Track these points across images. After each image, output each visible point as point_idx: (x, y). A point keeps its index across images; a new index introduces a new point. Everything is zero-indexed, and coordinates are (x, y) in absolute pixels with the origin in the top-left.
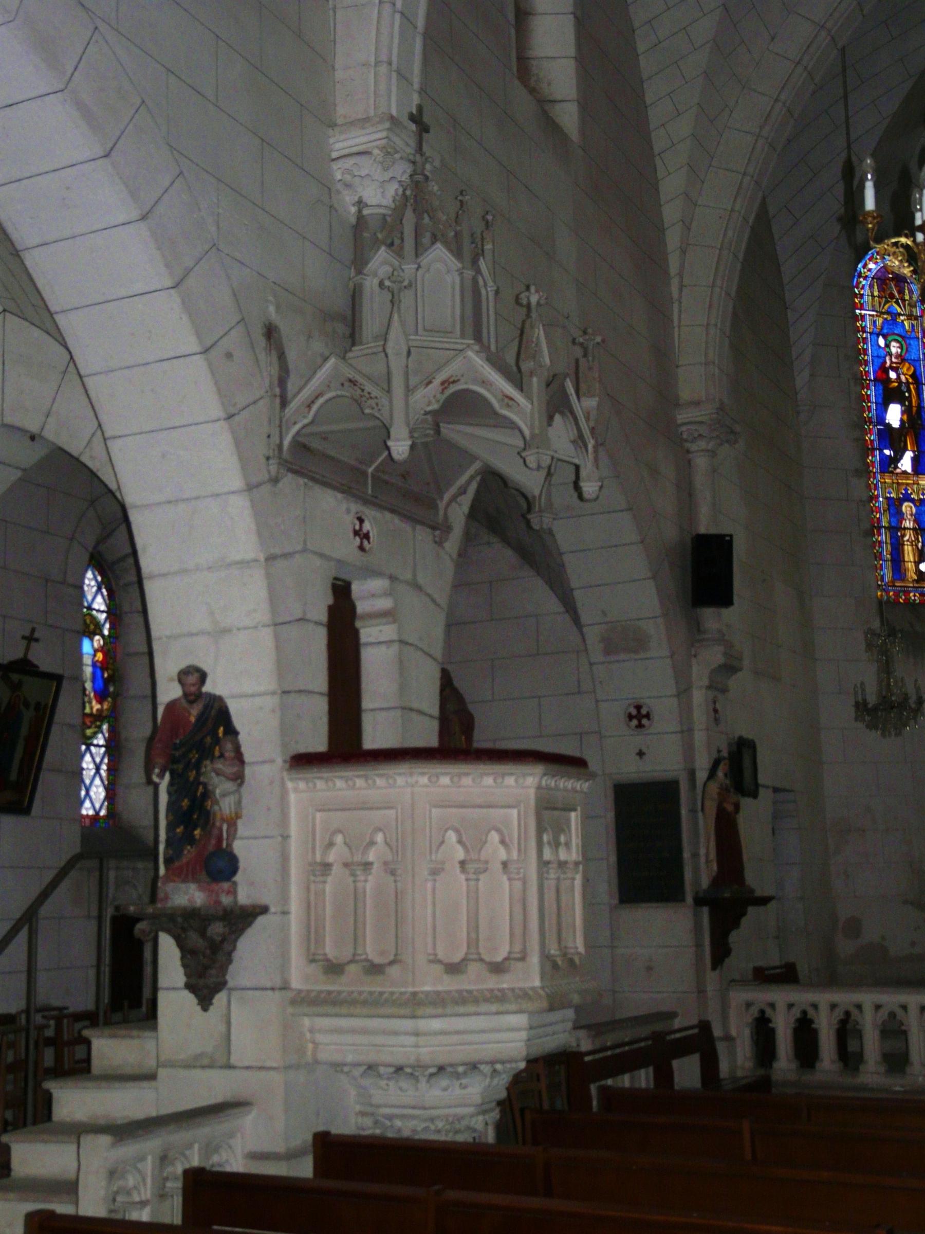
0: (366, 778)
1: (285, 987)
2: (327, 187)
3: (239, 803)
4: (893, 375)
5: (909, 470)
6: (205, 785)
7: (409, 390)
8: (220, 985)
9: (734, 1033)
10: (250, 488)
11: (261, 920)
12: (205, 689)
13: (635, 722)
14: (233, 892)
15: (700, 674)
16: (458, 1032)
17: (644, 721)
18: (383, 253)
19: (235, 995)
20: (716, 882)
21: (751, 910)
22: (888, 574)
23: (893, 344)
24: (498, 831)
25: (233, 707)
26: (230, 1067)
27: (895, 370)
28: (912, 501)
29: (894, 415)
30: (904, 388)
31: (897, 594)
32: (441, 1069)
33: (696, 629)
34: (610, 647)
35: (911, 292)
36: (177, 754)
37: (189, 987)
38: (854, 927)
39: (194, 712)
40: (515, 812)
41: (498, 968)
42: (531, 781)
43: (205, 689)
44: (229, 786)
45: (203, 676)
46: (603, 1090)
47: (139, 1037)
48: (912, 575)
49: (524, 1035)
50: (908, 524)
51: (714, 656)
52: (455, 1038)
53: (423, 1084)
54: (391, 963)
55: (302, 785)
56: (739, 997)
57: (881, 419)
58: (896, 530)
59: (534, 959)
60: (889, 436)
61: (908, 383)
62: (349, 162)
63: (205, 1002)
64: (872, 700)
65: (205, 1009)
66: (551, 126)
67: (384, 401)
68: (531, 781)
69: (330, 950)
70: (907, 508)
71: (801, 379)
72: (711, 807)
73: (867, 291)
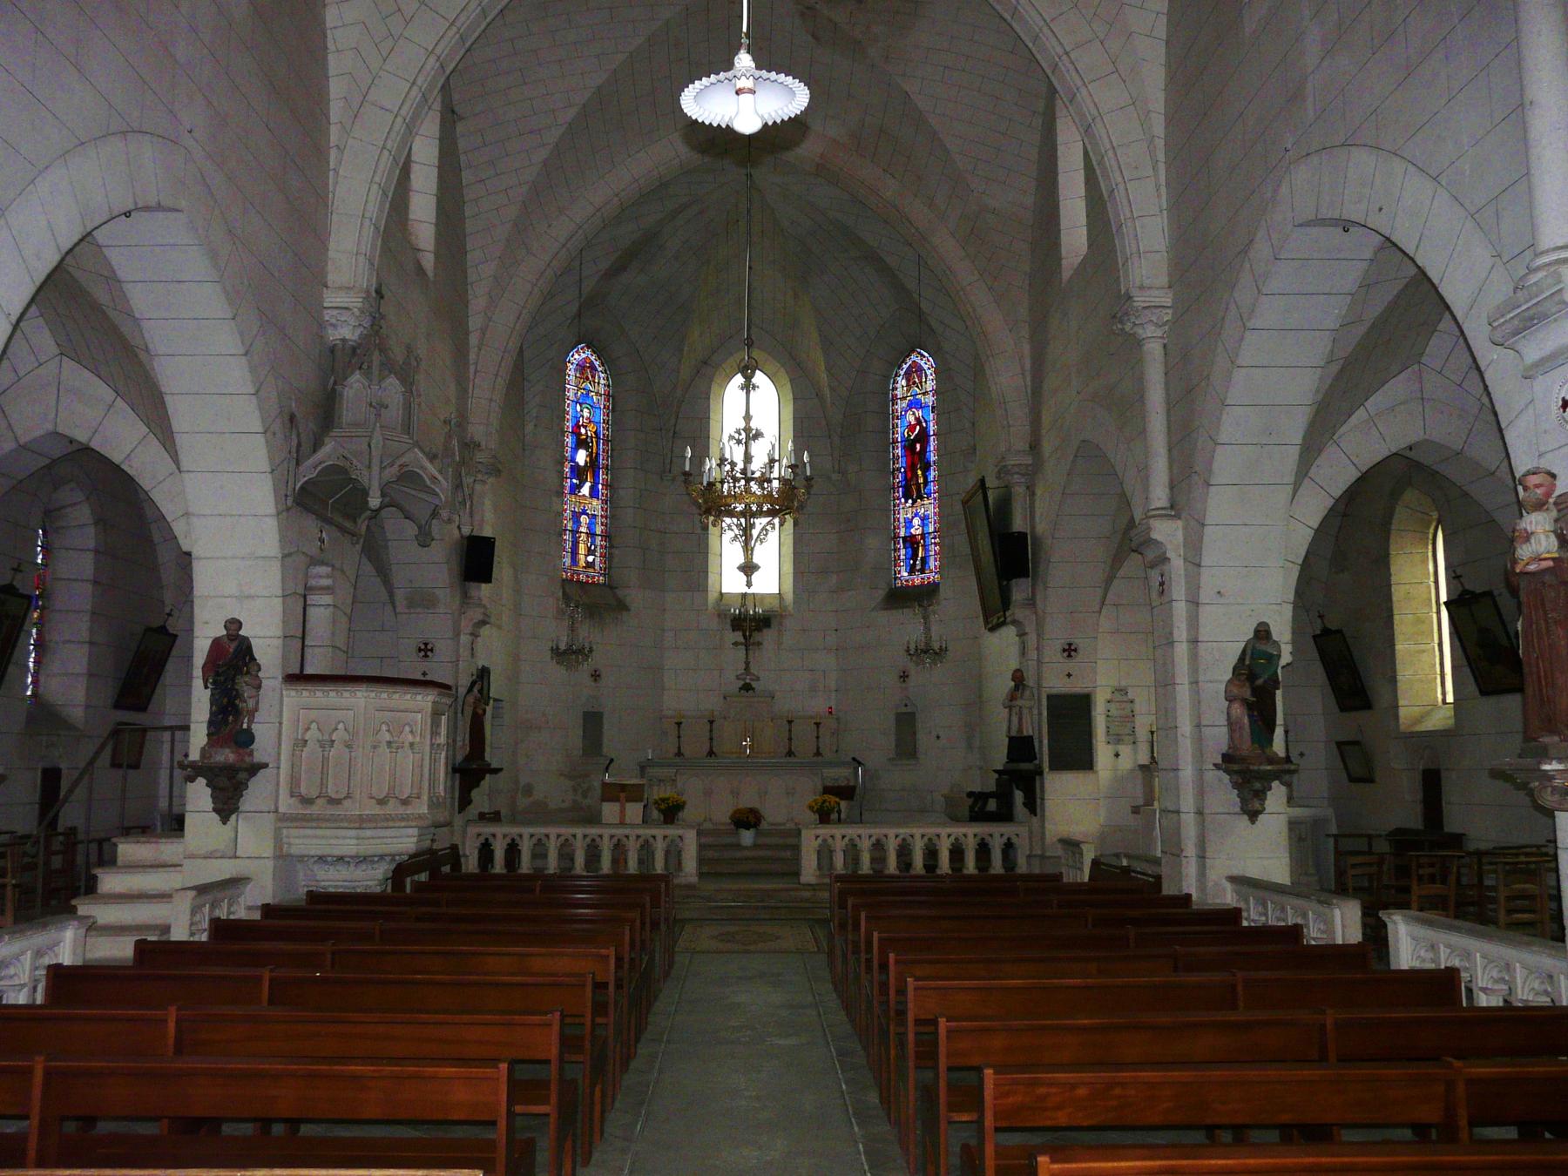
0: (337, 692)
1: (276, 811)
2: (322, 325)
3: (257, 703)
4: (583, 431)
5: (587, 494)
6: (237, 690)
7: (382, 469)
8: (235, 810)
9: (468, 853)
10: (278, 514)
11: (262, 773)
12: (241, 633)
13: (423, 653)
14: (251, 754)
15: (466, 625)
16: (379, 838)
17: (429, 653)
18: (357, 376)
19: (242, 816)
20: (467, 759)
21: (488, 776)
22: (568, 561)
23: (585, 410)
24: (410, 726)
25: (253, 642)
26: (236, 857)
27: (585, 427)
28: (587, 514)
29: (581, 457)
30: (589, 440)
31: (572, 575)
32: (365, 858)
33: (465, 595)
34: (411, 603)
35: (599, 377)
36: (220, 671)
37: (215, 810)
38: (528, 790)
39: (232, 647)
40: (420, 715)
41: (405, 802)
42: (430, 698)
43: (241, 633)
44: (253, 692)
45: (239, 624)
46: (412, 881)
47: (156, 842)
48: (582, 563)
49: (415, 840)
50: (583, 529)
51: (476, 614)
52: (379, 841)
53: (352, 868)
54: (345, 798)
55: (293, 693)
56: (472, 830)
57: (573, 460)
58: (575, 532)
59: (425, 797)
60: (578, 472)
61: (592, 437)
62: (335, 312)
63: (225, 820)
64: (563, 647)
65: (224, 823)
66: (420, 270)
67: (365, 472)
68: (430, 698)
69: (303, 790)
70: (584, 519)
71: (530, 427)
72: (469, 711)
73: (571, 370)
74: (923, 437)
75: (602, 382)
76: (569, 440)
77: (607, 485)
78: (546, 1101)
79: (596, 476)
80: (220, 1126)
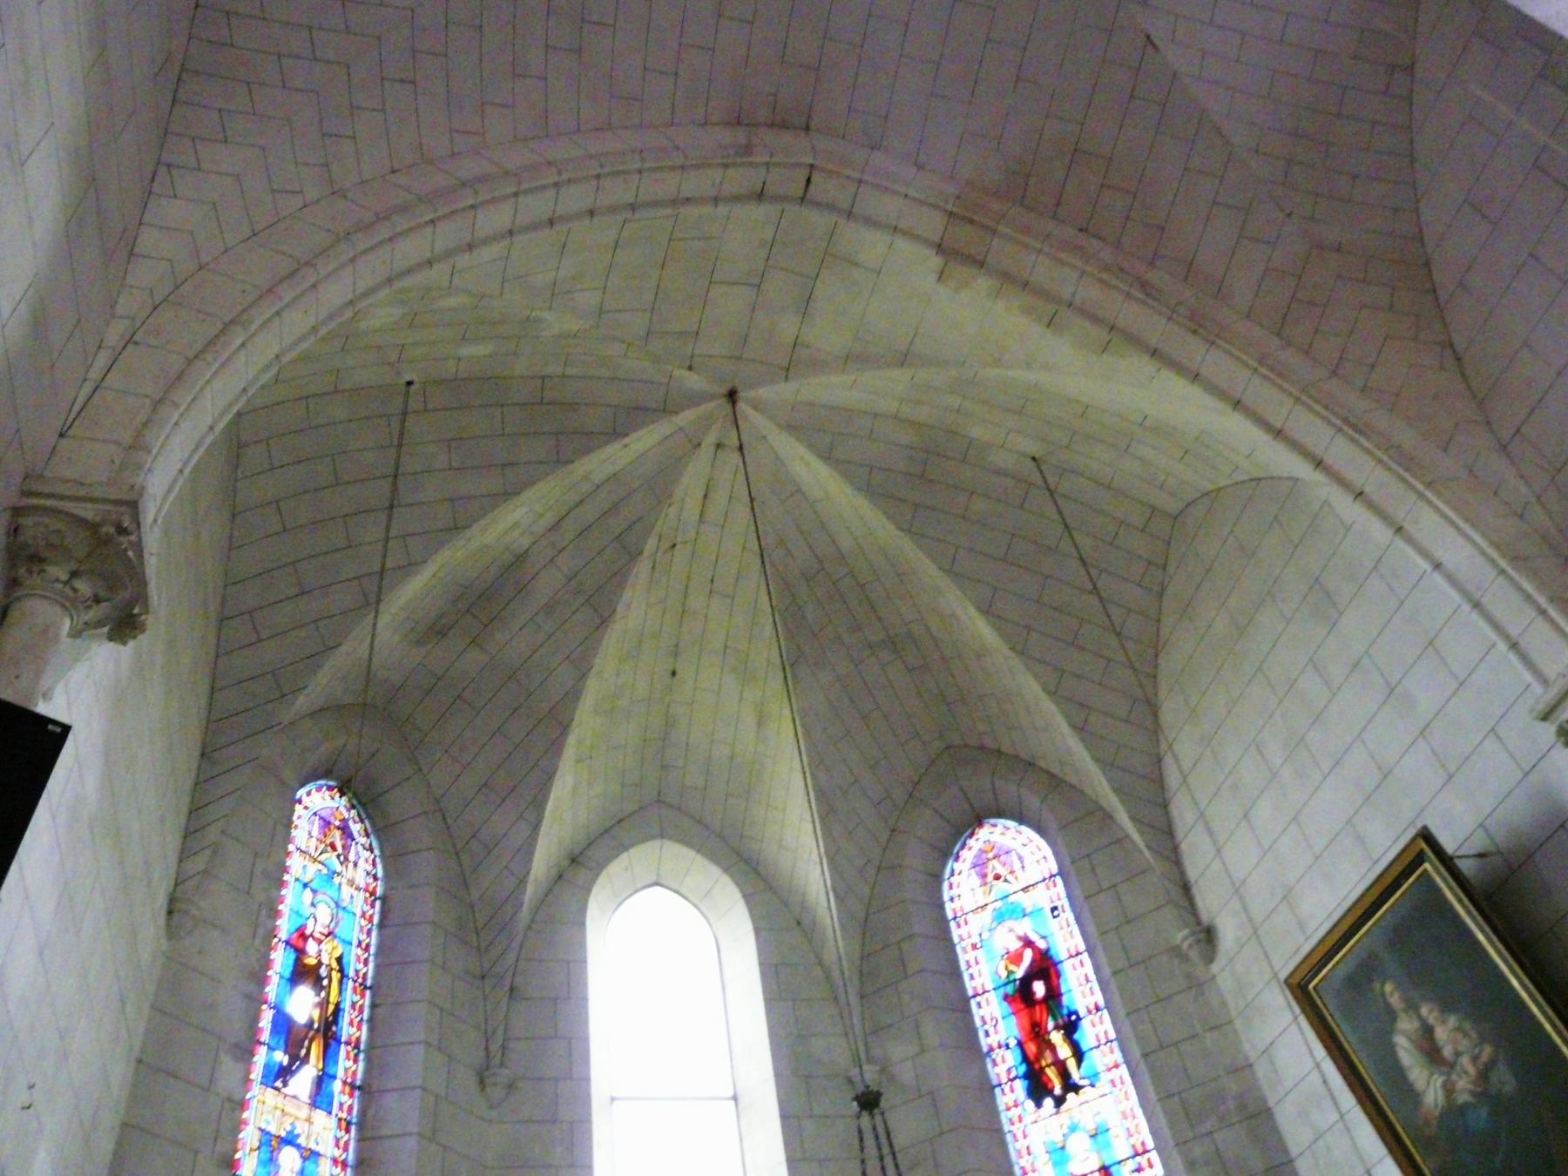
4: (311, 947)
30: (323, 972)
60: (292, 1038)
74: (1045, 967)
75: (361, 863)
76: (281, 960)
77: (353, 1087)
78: (1425, 871)
79: (328, 1054)
80: (305, 966)
